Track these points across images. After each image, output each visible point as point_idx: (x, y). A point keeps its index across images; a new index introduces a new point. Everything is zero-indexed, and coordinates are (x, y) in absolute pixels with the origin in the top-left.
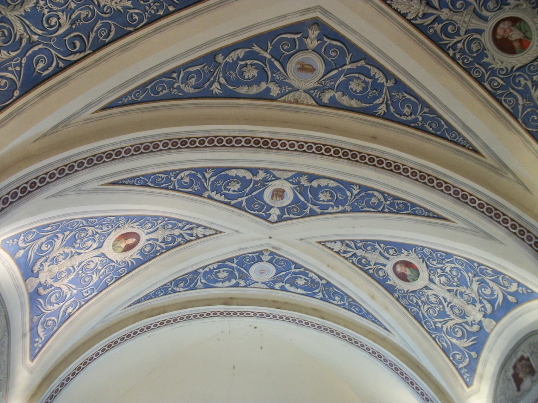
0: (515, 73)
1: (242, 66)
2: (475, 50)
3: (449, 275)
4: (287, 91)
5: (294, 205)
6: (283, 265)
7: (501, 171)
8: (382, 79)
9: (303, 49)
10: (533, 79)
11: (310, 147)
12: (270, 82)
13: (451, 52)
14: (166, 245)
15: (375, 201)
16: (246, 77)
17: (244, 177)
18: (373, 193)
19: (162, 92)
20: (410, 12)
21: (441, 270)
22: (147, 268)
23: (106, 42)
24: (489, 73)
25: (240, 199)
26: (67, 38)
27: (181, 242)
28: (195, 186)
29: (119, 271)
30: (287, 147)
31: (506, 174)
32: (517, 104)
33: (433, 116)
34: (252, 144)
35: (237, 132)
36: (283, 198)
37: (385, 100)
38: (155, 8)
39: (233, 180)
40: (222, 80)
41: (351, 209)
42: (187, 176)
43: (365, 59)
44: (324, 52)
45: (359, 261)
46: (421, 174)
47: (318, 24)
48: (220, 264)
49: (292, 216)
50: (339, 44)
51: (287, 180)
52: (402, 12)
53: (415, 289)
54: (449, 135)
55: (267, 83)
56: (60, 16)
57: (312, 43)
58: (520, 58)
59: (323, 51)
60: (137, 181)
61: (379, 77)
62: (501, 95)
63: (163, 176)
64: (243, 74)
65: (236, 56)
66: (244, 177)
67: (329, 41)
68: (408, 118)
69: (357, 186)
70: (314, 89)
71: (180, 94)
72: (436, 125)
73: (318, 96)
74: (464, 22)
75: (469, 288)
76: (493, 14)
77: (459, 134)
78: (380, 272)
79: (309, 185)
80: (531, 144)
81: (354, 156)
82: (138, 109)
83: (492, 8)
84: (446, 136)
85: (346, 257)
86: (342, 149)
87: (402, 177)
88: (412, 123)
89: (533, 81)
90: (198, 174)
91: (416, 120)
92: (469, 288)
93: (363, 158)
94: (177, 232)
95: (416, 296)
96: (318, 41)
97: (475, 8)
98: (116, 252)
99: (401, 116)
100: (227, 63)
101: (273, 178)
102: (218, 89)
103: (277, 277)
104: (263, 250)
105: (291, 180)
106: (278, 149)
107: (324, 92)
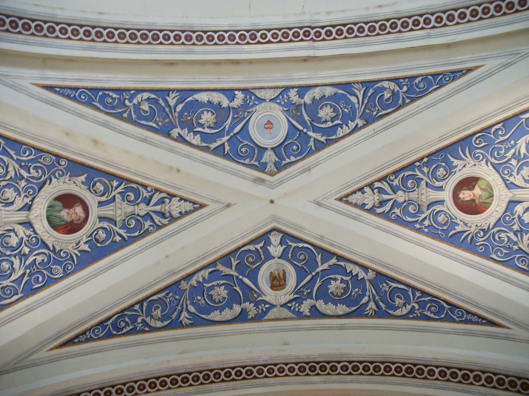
2: (98, 184)
3: (10, 256)
5: (254, 267)
6: (242, 148)
11: (260, 372)
12: (302, 104)
14: (414, 173)
15: (156, 312)
17: (326, 303)
18: (163, 322)
21: (25, 255)
22: (442, 139)
25: (326, 266)
27: (394, 177)
28: (387, 289)
29: (484, 144)
30: (286, 368)
34: (328, 366)
35: (348, 380)
36: (270, 276)
39: (339, 297)
41: (180, 287)
42: (398, 308)
45: (137, 194)
48: (334, 137)
49: (251, 247)
51: (273, 306)
53: (42, 192)
60: (462, 316)
63: (428, 314)
64: (334, 109)
69: (185, 324)
73: (248, 97)
78: (102, 188)
79: (244, 305)
81: (207, 377)
85: (158, 193)
86: (223, 381)
87: (142, 378)
90: (384, 309)
91: (131, 101)
93: (196, 379)
94: (401, 197)
95: (35, 181)
98: (488, 182)
101: (289, 305)
103: (244, 118)
104: (277, 173)
105: (267, 306)
106: (297, 364)
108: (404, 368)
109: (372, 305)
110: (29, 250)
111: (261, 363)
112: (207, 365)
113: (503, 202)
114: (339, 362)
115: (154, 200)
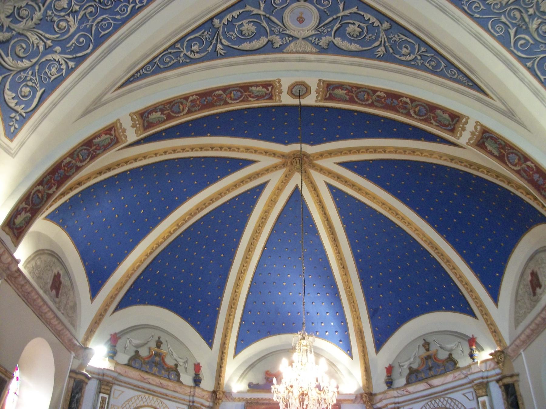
3: (64, 16)
21: (76, 12)
25: (347, 12)
28: (397, 40)
51: (295, 38)
66: (343, 40)
75: (34, 26)
92: (34, 26)
109: (382, 49)
110: (79, 7)
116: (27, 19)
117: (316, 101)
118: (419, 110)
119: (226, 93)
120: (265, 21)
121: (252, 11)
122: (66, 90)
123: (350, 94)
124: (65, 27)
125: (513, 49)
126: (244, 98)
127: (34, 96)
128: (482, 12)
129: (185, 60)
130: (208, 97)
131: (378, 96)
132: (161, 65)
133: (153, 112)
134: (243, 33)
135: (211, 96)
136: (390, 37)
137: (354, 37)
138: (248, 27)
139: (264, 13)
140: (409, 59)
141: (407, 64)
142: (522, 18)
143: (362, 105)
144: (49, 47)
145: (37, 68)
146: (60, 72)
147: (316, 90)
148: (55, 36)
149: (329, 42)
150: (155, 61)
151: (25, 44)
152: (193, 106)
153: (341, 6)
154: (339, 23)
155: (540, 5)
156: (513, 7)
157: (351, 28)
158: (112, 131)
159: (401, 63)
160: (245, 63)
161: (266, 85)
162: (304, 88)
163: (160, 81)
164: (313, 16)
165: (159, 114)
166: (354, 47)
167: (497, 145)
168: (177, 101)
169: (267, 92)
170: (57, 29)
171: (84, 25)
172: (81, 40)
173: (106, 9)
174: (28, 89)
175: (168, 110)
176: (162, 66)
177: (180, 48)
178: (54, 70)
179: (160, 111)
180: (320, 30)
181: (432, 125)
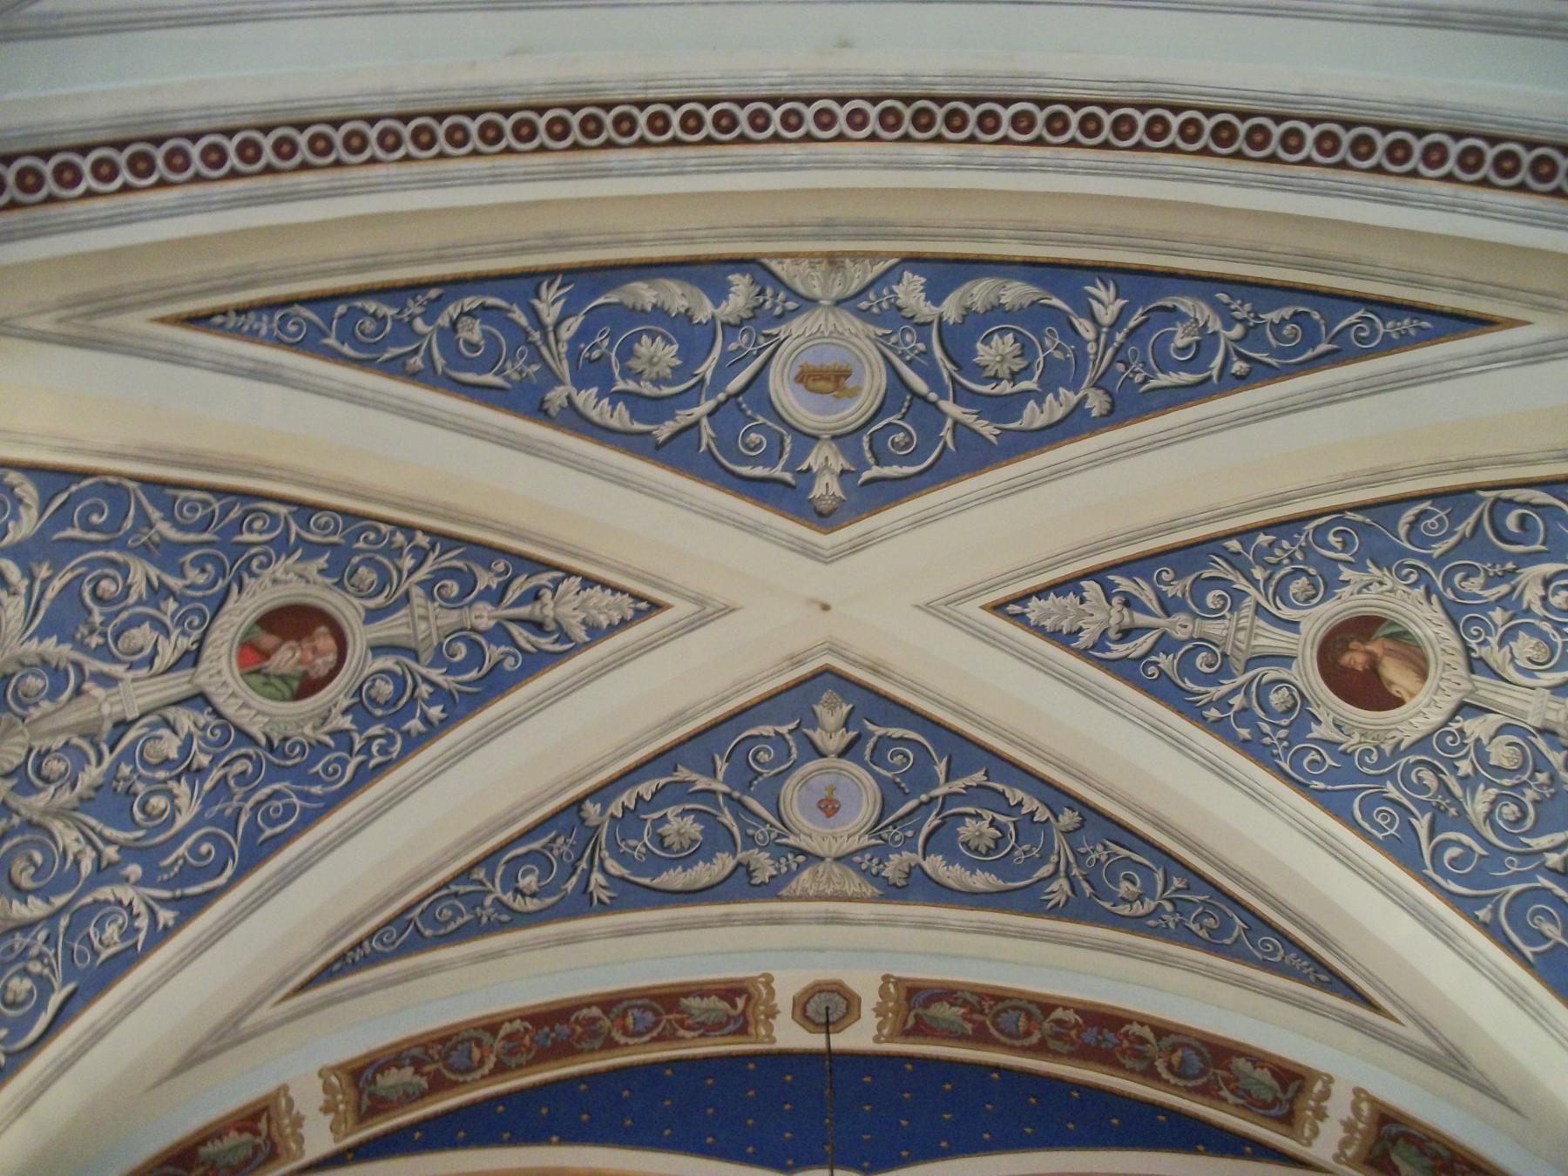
0: (226, 581)
1: (1026, 372)
2: (363, 570)
3: (165, 781)
4: (872, 296)
7: (80, 316)
8: (586, 399)
9: (848, 439)
10: (176, 600)
11: (759, 121)
12: (931, 323)
13: (422, 540)
16: (1010, 337)
17: (950, 863)
19: (1283, 319)
20: (578, 593)
21: (199, 770)
23: (1429, 502)
24: (293, 538)
25: (958, 785)
26: (1538, 547)
28: (1103, 858)
31: (60, 321)
32: (169, 517)
33: (387, 356)
37: (551, 337)
38: (1277, 552)
40: (1085, 328)
43: (659, 447)
44: (782, 442)
46: (331, 158)
47: (820, 514)
50: (746, 470)
51: (812, 858)
52: (598, 588)
53: (222, 620)
54: (306, 320)
55: (940, 318)
56: (1539, 603)
57: (825, 461)
58: (238, 620)
59: (788, 440)
61: (598, 402)
62: (226, 511)
64: (1023, 347)
65: (1046, 406)
67: (777, 472)
68: (458, 310)
70: (783, 317)
71: (1223, 297)
72: (362, 333)
73: (769, 291)
74: (425, 618)
76: (367, 672)
77: (279, 343)
80: (55, 449)
81: (592, 127)
82: (1372, 277)
83: (378, 683)
84: (312, 310)
86: (643, 143)
88: (439, 298)
89: (171, 593)
91: (429, 318)
92: (76, 804)
93: (559, 129)
96: (809, 469)
97: (417, 659)
99: (483, 307)
100: (1075, 387)
102: (1099, 301)
106: (874, 100)
107: (754, 309)
108: (1209, 124)
109: (1061, 884)
110: (210, 758)
111: (764, 92)
112: (593, 86)
113: (1436, 710)
114: (1006, 102)
115: (513, 594)
116: (59, 783)
117: (877, 1039)
118: (1183, 1061)
119: (612, 1016)
120: (731, 813)
121: (693, 783)
122: (138, 991)
123: (976, 1017)
124: (164, 811)
125: (1430, 872)
126: (664, 1028)
127: (41, 1006)
128: (1330, 776)
129: (496, 915)
130: (557, 1026)
131: (1060, 1022)
132: (426, 928)
133: (389, 1068)
134: (667, 842)
135: (567, 1021)
136: (1082, 850)
137: (980, 854)
138: (681, 826)
139: (726, 789)
140: (1141, 911)
141: (1135, 925)
142: (1444, 788)
143: (1011, 1049)
144: (110, 864)
145: (64, 922)
146: (129, 938)
147: (875, 1006)
148: (131, 835)
149: (910, 867)
150: (409, 916)
151: (44, 854)
152: (512, 1053)
153: (941, 768)
154: (938, 815)
155: (1487, 749)
156: (1413, 758)
157: (971, 828)
158: (260, 1121)
159: (1116, 922)
160: (672, 927)
161: (731, 991)
162: (841, 1000)
163: (420, 973)
164: (864, 797)
165: (408, 1072)
166: (981, 881)
167: (1428, 1162)
168: (466, 1035)
169: (732, 1012)
170: (138, 816)
171: (217, 808)
172: (204, 848)
173: (284, 767)
174: (27, 984)
175: (434, 1062)
176: (428, 933)
177: (485, 880)
178: (112, 931)
179: (410, 1065)
180: (884, 834)
181: (1224, 1106)
